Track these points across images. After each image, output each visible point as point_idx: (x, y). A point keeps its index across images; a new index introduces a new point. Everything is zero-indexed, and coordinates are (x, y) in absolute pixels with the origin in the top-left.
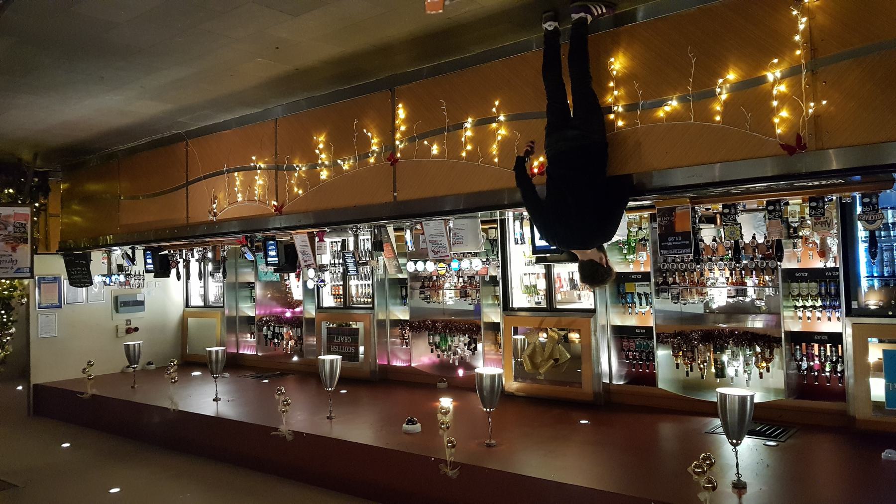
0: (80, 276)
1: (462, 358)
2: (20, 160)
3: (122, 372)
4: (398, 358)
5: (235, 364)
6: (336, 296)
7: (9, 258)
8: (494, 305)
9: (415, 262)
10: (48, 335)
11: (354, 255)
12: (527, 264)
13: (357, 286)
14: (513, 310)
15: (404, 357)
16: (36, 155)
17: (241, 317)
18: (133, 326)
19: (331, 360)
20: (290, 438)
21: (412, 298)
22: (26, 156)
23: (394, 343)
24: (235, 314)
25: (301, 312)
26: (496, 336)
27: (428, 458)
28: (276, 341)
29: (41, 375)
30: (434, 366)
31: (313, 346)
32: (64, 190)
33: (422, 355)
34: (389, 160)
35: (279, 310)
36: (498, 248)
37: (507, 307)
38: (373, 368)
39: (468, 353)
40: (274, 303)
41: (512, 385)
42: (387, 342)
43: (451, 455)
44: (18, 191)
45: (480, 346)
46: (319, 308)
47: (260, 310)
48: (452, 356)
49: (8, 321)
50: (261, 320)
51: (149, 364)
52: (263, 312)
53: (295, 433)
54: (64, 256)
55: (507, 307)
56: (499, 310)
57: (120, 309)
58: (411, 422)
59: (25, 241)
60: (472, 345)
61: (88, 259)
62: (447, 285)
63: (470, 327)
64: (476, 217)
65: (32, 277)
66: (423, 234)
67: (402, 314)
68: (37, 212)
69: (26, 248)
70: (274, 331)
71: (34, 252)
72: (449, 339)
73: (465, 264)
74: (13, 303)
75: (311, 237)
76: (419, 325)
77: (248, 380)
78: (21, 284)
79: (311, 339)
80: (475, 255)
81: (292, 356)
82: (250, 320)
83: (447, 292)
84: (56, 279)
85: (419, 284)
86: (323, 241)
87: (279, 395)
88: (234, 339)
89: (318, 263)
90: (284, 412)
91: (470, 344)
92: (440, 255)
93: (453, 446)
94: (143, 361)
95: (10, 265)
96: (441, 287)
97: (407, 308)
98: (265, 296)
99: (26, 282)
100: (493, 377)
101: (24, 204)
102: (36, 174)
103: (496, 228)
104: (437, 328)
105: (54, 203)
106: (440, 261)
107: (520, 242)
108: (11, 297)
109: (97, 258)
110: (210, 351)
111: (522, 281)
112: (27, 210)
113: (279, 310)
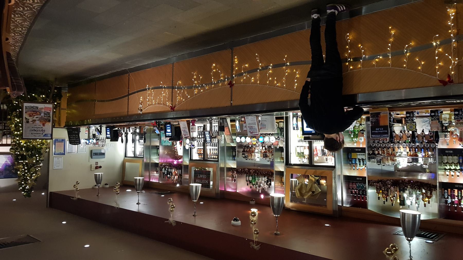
0: (75, 140)
1: (263, 189)
2: (48, 81)
3: (93, 188)
4: (230, 187)
5: (148, 186)
6: (199, 154)
7: (41, 129)
8: (281, 162)
9: (241, 137)
10: (58, 168)
11: (209, 133)
12: (299, 141)
13: (210, 150)
14: (291, 165)
15: (233, 187)
16: (56, 79)
17: (152, 163)
18: (99, 165)
19: (196, 186)
20: (174, 224)
21: (238, 157)
22: (51, 79)
23: (228, 180)
24: (149, 162)
25: (182, 162)
26: (281, 178)
27: (244, 239)
28: (169, 176)
29: (54, 187)
30: (248, 192)
31: (187, 179)
32: (69, 97)
33: (242, 187)
34: (229, 84)
35: (171, 160)
36: (284, 132)
37: (288, 163)
38: (217, 192)
39: (266, 186)
40: (168, 157)
41: (289, 204)
42: (224, 179)
43: (256, 238)
44: (47, 96)
45: (273, 183)
46: (191, 160)
47: (161, 160)
48: (258, 188)
49: (40, 160)
50: (161, 165)
51: (106, 184)
52: (162, 161)
53: (177, 223)
54: (67, 129)
55: (288, 163)
56: (283, 165)
57: (93, 157)
58: (236, 220)
59: (49, 121)
60: (268, 182)
61: (78, 131)
62: (256, 151)
63: (268, 173)
64: (273, 115)
65: (52, 139)
66: (245, 123)
67: (232, 164)
68: (55, 107)
69: (49, 125)
70: (168, 171)
71: (53, 127)
72: (257, 179)
73: (266, 139)
74: (42, 151)
75: (188, 123)
76: (241, 171)
77: (154, 195)
78: (46, 142)
79: (186, 176)
80: (272, 135)
81: (176, 184)
82: (156, 165)
83: (257, 154)
84: (63, 141)
85: (242, 150)
86: (194, 125)
87: (170, 202)
88: (148, 174)
89: (192, 136)
90: (171, 211)
91: (267, 182)
92: (253, 134)
93: (257, 233)
94: (103, 183)
95: (41, 132)
96: (253, 152)
97: (235, 162)
98: (164, 153)
99: (49, 141)
100: (279, 199)
101: (49, 103)
102: (56, 88)
103: (283, 122)
104: (250, 173)
105: (64, 103)
106: (253, 137)
107: (296, 129)
108: (41, 148)
109: (83, 131)
110: (136, 179)
111: (296, 150)
112: (51, 106)
113: (171, 160)
